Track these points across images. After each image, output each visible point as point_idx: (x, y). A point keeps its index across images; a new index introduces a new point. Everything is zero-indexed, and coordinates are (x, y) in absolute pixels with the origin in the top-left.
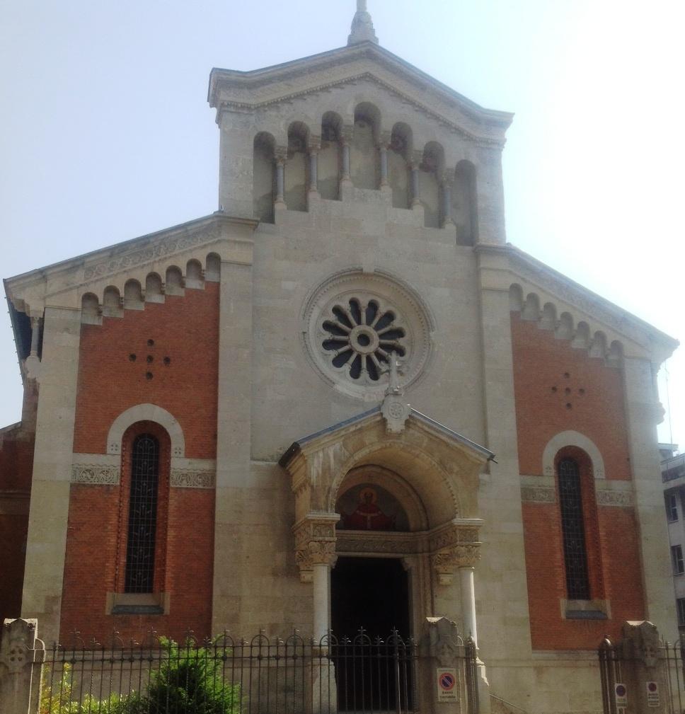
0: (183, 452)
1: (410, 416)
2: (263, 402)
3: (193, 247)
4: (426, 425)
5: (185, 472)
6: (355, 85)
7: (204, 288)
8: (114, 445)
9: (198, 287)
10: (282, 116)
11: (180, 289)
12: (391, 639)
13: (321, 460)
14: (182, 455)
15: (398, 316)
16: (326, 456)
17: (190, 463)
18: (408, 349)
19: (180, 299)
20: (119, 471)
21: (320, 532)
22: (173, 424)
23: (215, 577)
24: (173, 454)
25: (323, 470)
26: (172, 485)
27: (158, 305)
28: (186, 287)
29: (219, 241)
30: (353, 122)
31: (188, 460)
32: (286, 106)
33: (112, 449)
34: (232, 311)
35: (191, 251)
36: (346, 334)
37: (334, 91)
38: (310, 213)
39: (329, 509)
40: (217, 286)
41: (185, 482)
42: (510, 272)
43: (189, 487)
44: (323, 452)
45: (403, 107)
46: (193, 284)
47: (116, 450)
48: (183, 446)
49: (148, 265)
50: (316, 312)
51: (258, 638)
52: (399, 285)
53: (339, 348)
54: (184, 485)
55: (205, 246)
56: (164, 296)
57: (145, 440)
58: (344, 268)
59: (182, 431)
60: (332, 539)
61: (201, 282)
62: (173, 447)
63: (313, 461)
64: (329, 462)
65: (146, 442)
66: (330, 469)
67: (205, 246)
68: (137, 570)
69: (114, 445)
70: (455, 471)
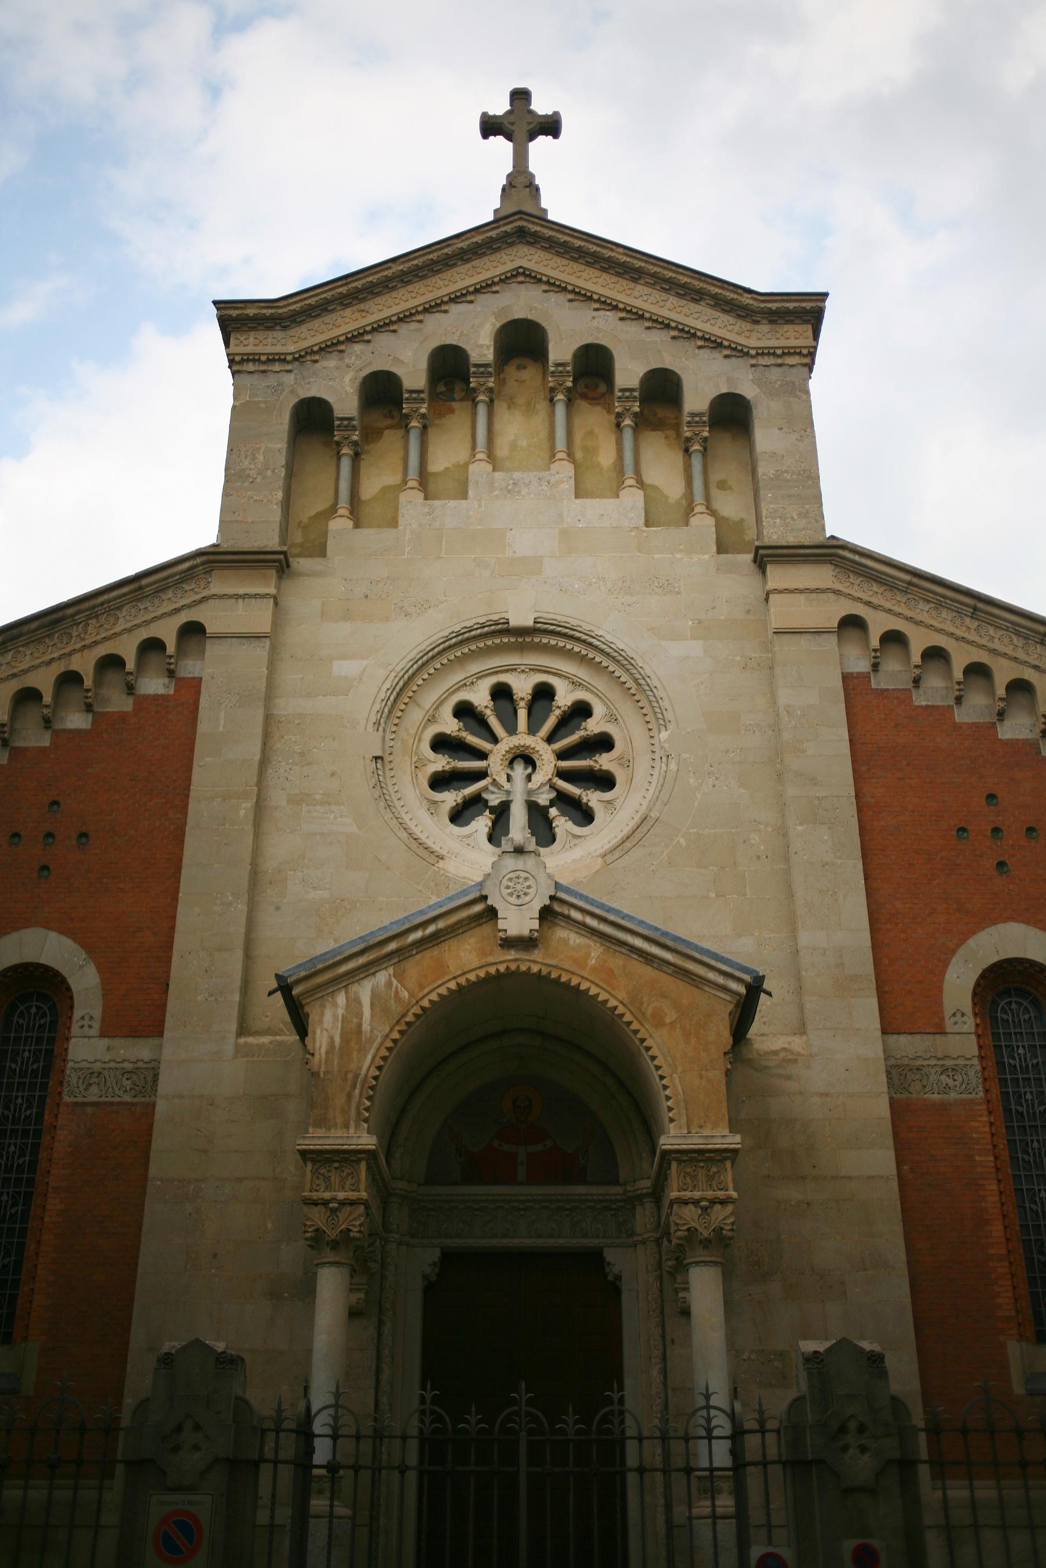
0: (97, 1025)
1: (552, 898)
2: (278, 908)
3: (153, 615)
4: (593, 915)
5: (98, 1066)
6: (496, 292)
7: (172, 692)
8: (87, 1018)
9: (161, 691)
10: (348, 366)
11: (124, 697)
12: (605, 1419)
13: (341, 1012)
14: (95, 1031)
15: (598, 709)
16: (354, 1003)
17: (108, 1049)
18: (620, 775)
19: (122, 717)
20: (979, 1068)
21: (327, 1179)
22: (81, 967)
23: (137, 1305)
24: (75, 1029)
25: (342, 1035)
26: (67, 1099)
27: (78, 732)
28: (138, 693)
29: (205, 599)
30: (962, 677)
31: (106, 1041)
32: (357, 348)
33: (90, 1027)
34: (221, 729)
35: (147, 623)
36: (483, 755)
37: (454, 308)
38: (400, 528)
39: (352, 1123)
40: (195, 685)
41: (94, 1089)
42: (837, 592)
43: (103, 1099)
44: (347, 993)
45: (594, 318)
46: (154, 685)
47: (90, 1027)
48: (97, 1013)
49: (60, 658)
50: (416, 716)
51: (331, 1411)
52: (591, 644)
53: (464, 788)
54: (93, 1095)
55: (177, 611)
56: (90, 716)
57: (31, 1006)
58: (468, 624)
59: (98, 980)
60: (353, 1195)
61: (166, 680)
62: (77, 1014)
63: (322, 1015)
64: (360, 1016)
65: (1014, 1006)
66: (359, 1031)
67: (177, 611)
68: (1029, 1139)
69: (87, 1018)
70: (668, 1020)
